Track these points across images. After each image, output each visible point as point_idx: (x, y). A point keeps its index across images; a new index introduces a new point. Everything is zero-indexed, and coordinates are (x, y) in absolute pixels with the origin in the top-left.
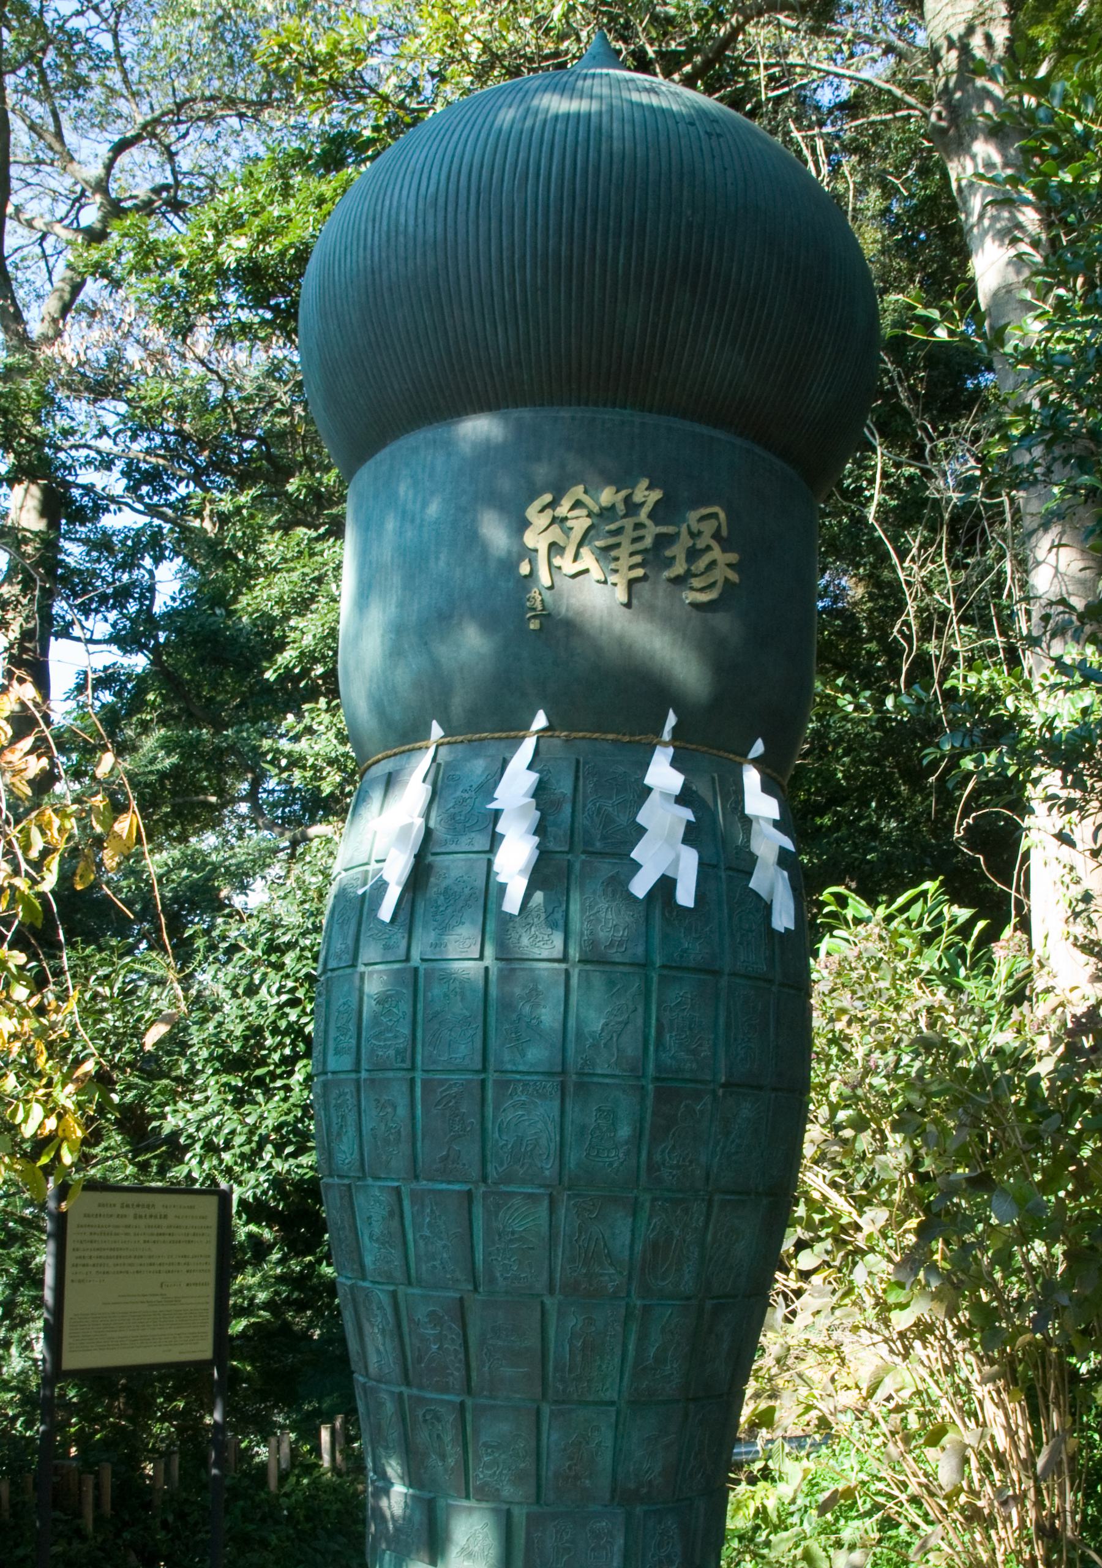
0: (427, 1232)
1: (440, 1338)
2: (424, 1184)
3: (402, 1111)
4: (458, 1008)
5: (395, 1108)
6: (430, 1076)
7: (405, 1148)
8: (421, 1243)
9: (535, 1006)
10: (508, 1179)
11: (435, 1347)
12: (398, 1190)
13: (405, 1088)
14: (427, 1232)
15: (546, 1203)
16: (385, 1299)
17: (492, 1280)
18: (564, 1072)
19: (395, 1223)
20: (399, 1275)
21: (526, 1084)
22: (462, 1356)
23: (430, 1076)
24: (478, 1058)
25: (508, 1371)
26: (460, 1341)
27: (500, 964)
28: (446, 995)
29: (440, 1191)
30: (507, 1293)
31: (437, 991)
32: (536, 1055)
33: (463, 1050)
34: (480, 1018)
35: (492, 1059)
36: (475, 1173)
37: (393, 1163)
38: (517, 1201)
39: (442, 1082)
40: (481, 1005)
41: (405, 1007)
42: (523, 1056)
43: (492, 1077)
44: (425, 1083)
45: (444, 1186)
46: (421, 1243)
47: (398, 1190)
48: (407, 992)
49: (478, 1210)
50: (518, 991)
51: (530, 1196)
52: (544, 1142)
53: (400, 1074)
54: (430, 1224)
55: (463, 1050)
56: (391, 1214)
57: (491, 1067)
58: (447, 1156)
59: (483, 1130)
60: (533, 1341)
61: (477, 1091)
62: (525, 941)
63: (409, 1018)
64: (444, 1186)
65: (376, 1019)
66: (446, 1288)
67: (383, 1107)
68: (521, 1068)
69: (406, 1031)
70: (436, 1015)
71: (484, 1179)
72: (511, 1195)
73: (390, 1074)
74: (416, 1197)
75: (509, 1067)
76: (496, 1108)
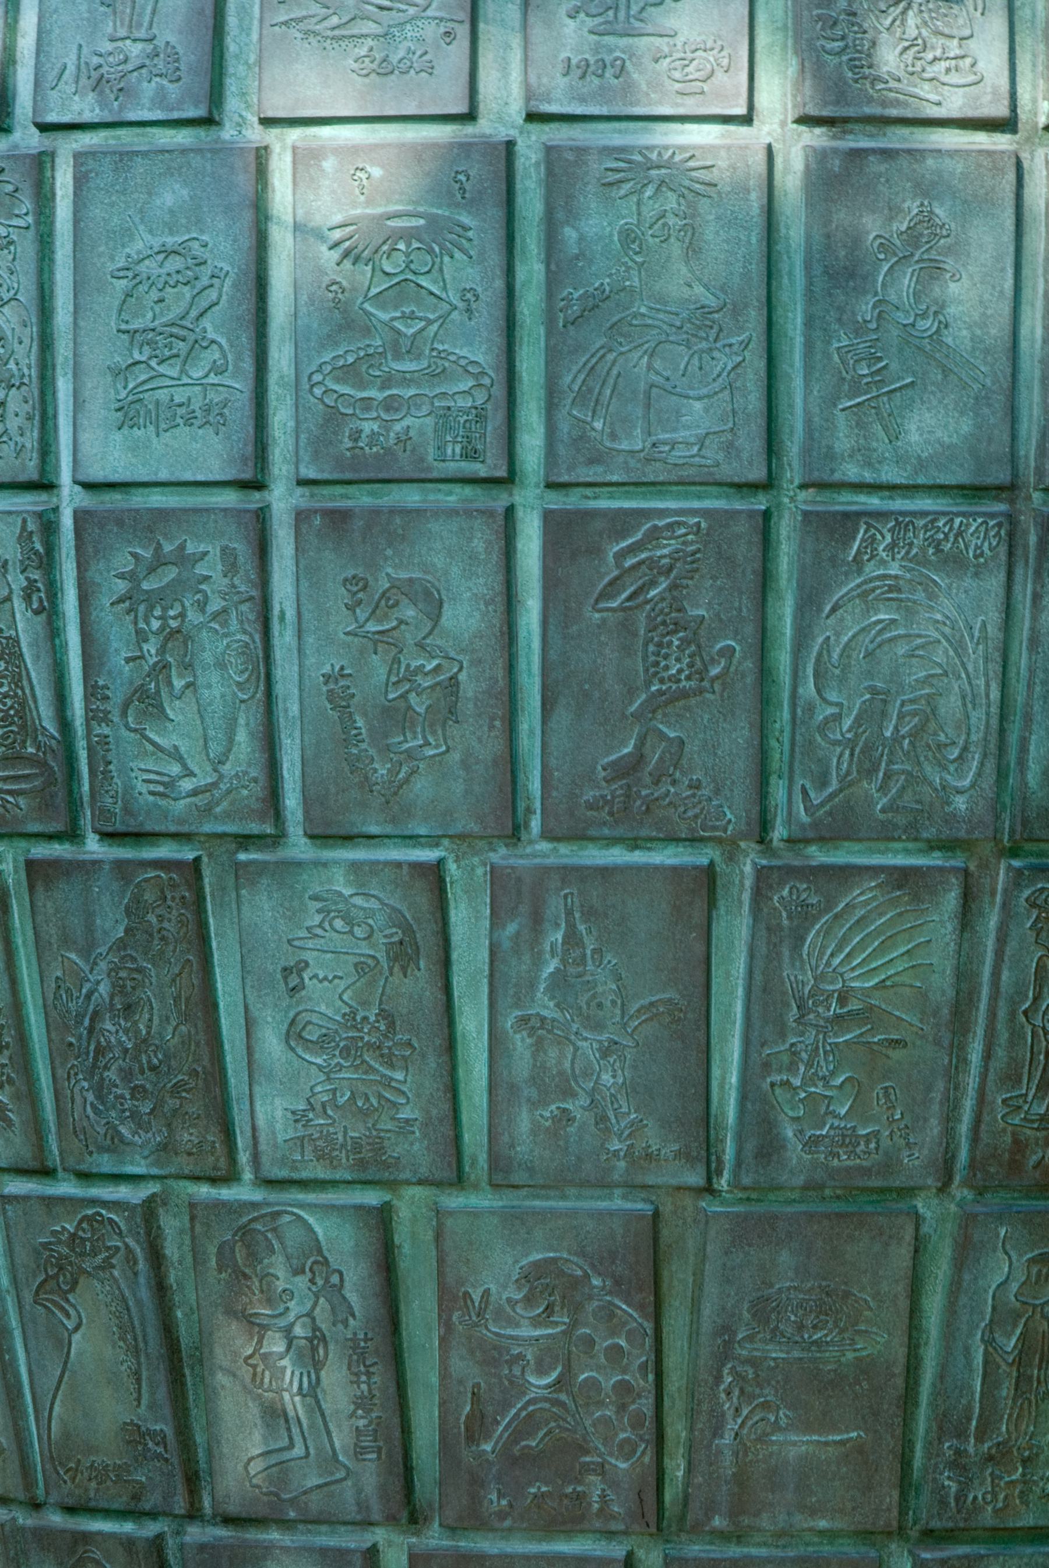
0: (544, 1006)
1: (559, 1355)
2: (539, 851)
3: (465, 617)
4: (681, 283)
5: (434, 606)
6: (573, 501)
7: (474, 738)
8: (520, 1043)
9: (933, 270)
10: (836, 828)
11: (539, 1382)
12: (434, 876)
13: (482, 540)
14: (544, 1006)
15: (951, 900)
16: (340, 1239)
17: (765, 1146)
18: (45, 485)
19: (417, 985)
20: (415, 1151)
21: (903, 522)
22: (646, 1405)
23: (573, 501)
24: (751, 442)
25: (796, 1445)
26: (642, 1356)
27: (816, 137)
28: (628, 237)
29: (605, 872)
30: (811, 1187)
31: (596, 224)
32: (932, 429)
33: (696, 417)
34: (754, 318)
35: (793, 447)
36: (734, 815)
37: (422, 787)
38: (862, 895)
39: (621, 523)
40: (756, 269)
41: (468, 273)
42: (894, 437)
43: (793, 503)
44: (560, 529)
45: (617, 856)
46: (520, 1043)
47: (434, 876)
48: (480, 226)
49: (735, 930)
50: (872, 226)
51: (903, 878)
52: (950, 706)
53: (454, 496)
54: (560, 982)
55: (696, 417)
56: (403, 954)
57: (792, 473)
58: (639, 759)
59: (764, 673)
60: (882, 1342)
61: (745, 551)
62: (889, 59)
63: (488, 313)
64: (617, 856)
65: (342, 317)
66: (603, 1184)
67: (384, 605)
68: (890, 474)
69: (480, 353)
70: (594, 304)
71: (761, 829)
72: (847, 874)
73: (411, 496)
74: (506, 893)
75: (851, 472)
76: (809, 603)
